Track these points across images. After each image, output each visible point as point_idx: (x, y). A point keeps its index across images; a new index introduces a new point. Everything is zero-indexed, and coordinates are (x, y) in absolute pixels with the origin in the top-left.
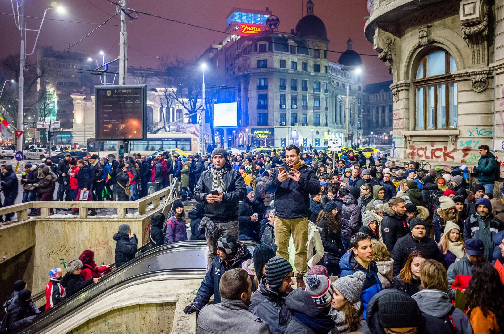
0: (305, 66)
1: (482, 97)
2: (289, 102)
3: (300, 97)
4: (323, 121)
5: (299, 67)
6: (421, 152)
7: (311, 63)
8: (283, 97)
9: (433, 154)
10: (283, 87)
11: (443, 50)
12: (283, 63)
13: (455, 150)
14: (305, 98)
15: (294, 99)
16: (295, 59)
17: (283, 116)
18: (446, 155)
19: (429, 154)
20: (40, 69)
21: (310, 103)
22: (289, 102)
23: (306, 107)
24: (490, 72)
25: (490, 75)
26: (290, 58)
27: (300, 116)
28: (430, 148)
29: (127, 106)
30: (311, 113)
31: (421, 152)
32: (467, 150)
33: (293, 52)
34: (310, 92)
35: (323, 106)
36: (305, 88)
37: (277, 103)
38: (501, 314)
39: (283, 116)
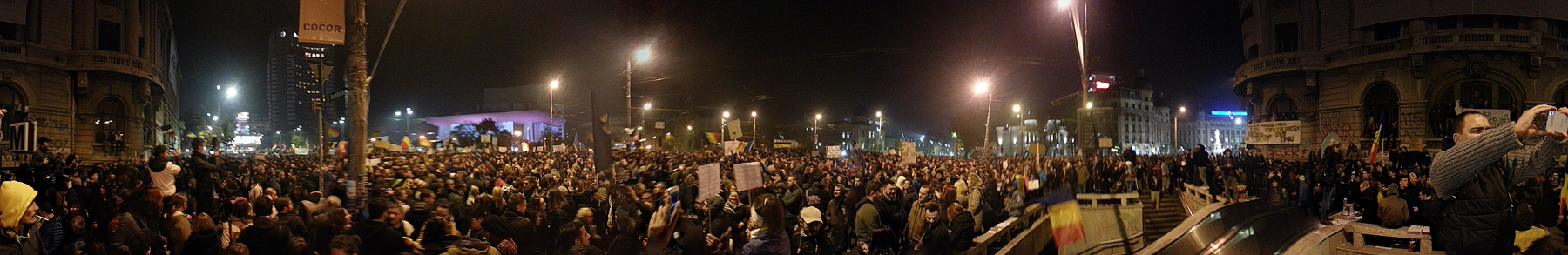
0: (1140, 107)
1: (1312, 123)
2: (1130, 129)
3: (1137, 126)
4: (1150, 140)
5: (1136, 107)
6: (1278, 153)
7: (1143, 104)
8: (1127, 126)
9: (1286, 153)
10: (1127, 119)
11: (1288, 98)
12: (1127, 104)
13: (1298, 151)
14: (1140, 126)
15: (1133, 126)
16: (1134, 102)
17: (1127, 137)
18: (1294, 154)
19: (1283, 154)
20: (1534, 133)
21: (1143, 129)
22: (1130, 129)
23: (1140, 132)
24: (1315, 112)
25: (1316, 113)
26: (1131, 102)
27: (1137, 137)
28: (1283, 150)
29: (539, 135)
30: (1143, 135)
31: (1278, 153)
32: (1304, 151)
33: (1133, 98)
34: (1143, 123)
35: (1150, 131)
36: (1140, 120)
37: (1123, 129)
38: (1417, 164)
39: (1127, 137)
